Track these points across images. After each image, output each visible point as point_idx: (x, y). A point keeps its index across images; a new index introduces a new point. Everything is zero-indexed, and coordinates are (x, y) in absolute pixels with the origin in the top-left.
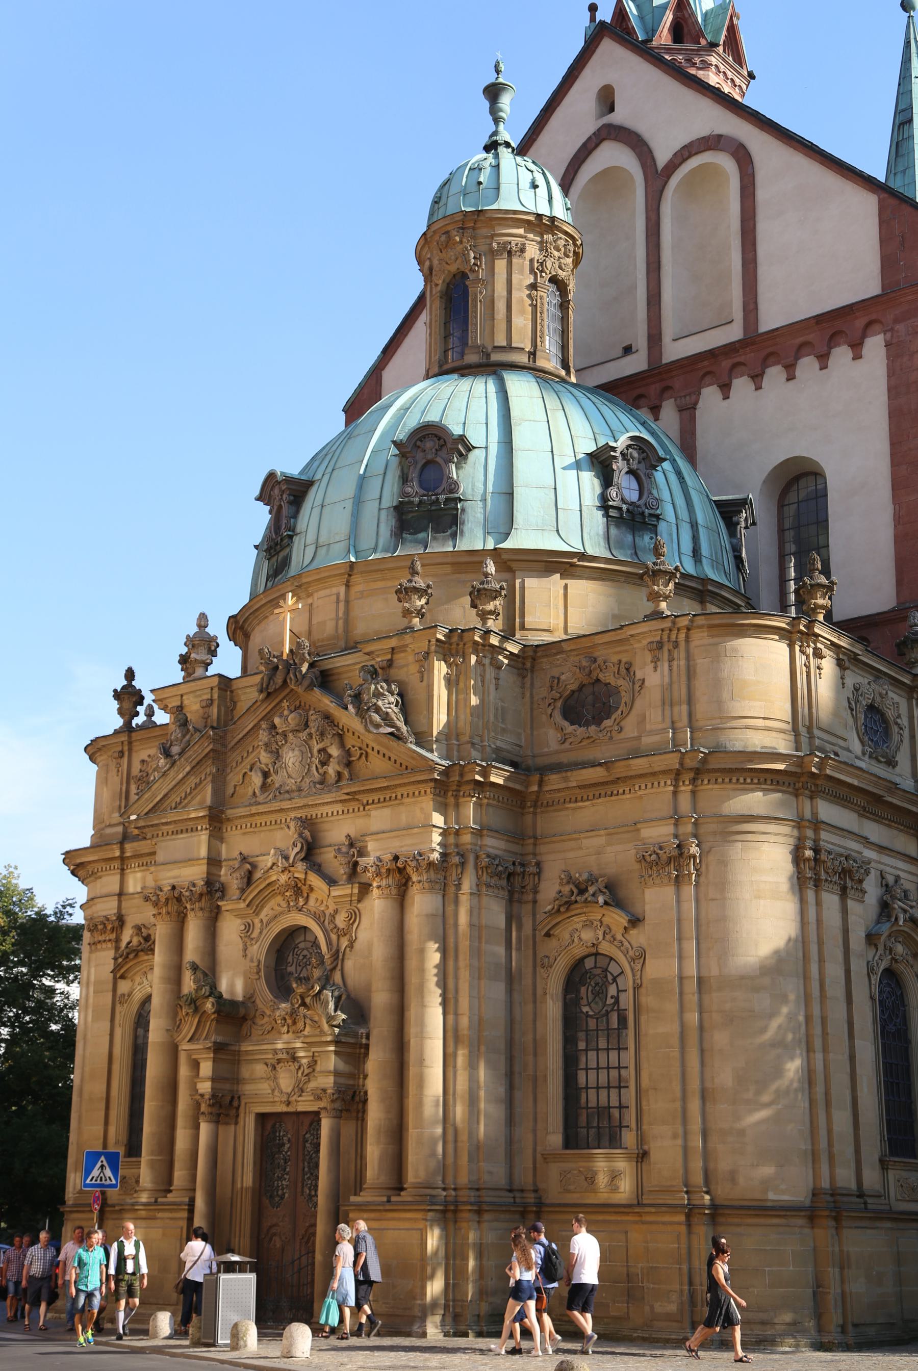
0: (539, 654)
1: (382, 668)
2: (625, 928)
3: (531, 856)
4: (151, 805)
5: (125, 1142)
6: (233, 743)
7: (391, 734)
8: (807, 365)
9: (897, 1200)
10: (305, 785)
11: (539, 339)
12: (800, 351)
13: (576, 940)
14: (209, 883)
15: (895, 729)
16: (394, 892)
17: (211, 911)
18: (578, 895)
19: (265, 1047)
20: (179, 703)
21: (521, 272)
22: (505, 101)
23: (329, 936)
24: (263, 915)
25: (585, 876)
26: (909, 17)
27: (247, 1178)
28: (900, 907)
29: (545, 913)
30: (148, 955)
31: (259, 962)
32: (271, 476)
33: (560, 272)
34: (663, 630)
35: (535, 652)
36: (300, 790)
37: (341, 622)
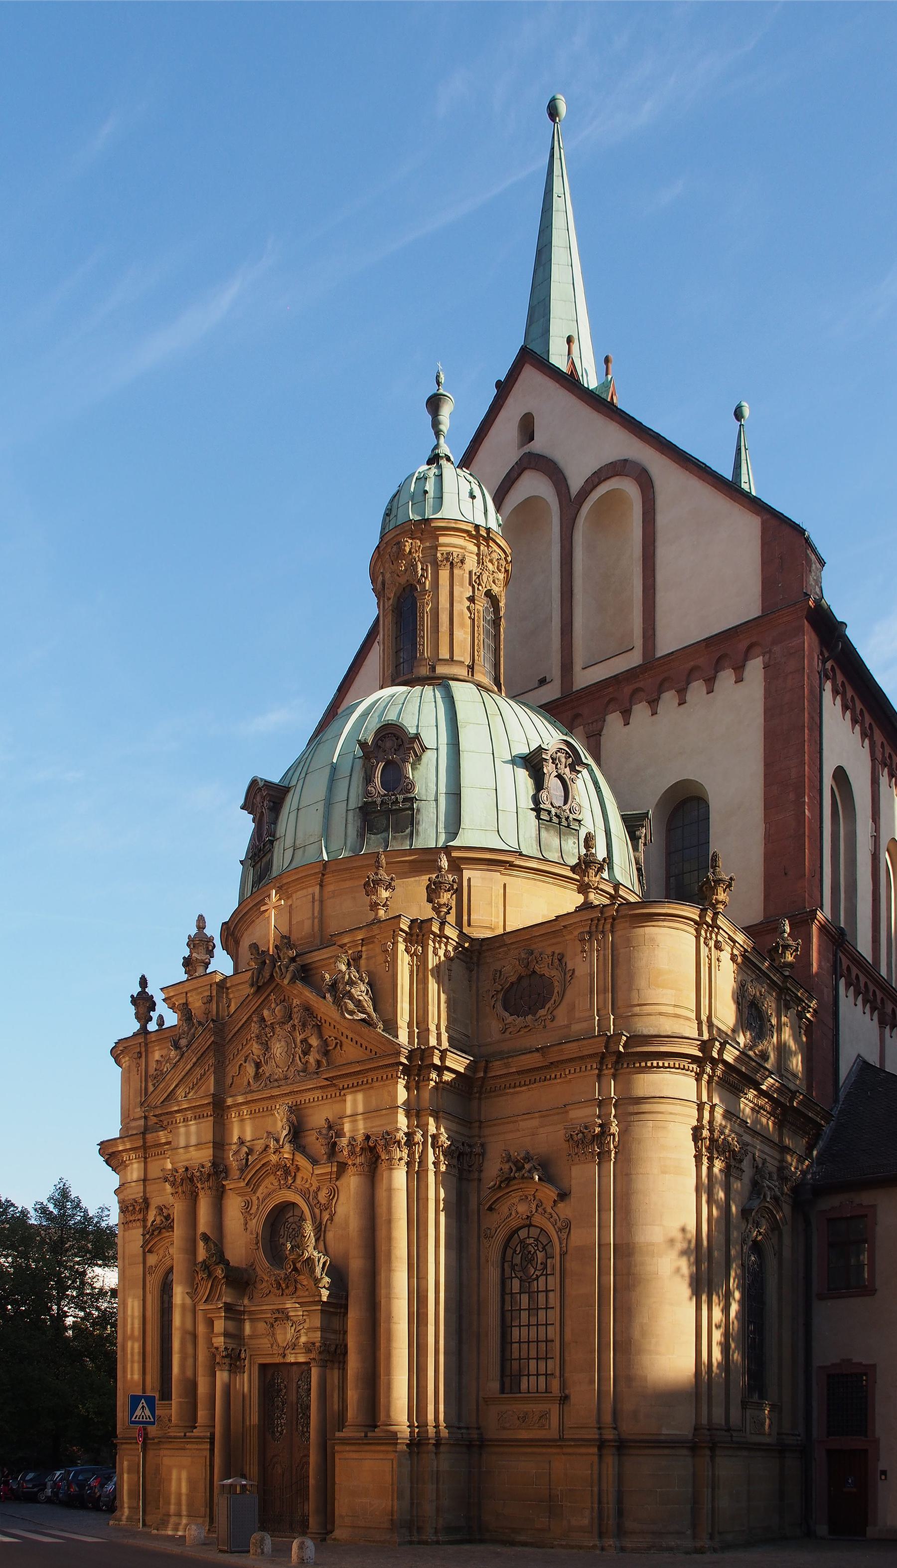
0: (484, 948)
1: (353, 960)
2: (555, 1201)
3: (477, 1138)
4: (166, 1095)
5: (159, 1389)
6: (230, 1036)
7: (363, 1020)
8: (697, 688)
9: (751, 1434)
10: (291, 1074)
11: (476, 653)
13: (513, 1214)
14: (214, 1164)
16: (366, 1169)
17: (217, 1190)
18: (516, 1172)
19: (264, 1308)
21: (462, 585)
22: (446, 412)
23: (313, 1210)
24: (258, 1194)
25: (522, 1155)
26: (740, 425)
27: (254, 1418)
28: (768, 1186)
29: (489, 1188)
30: (169, 1232)
31: (258, 1234)
32: (254, 782)
34: (592, 920)
35: (481, 946)
36: (286, 1078)
37: (316, 920)
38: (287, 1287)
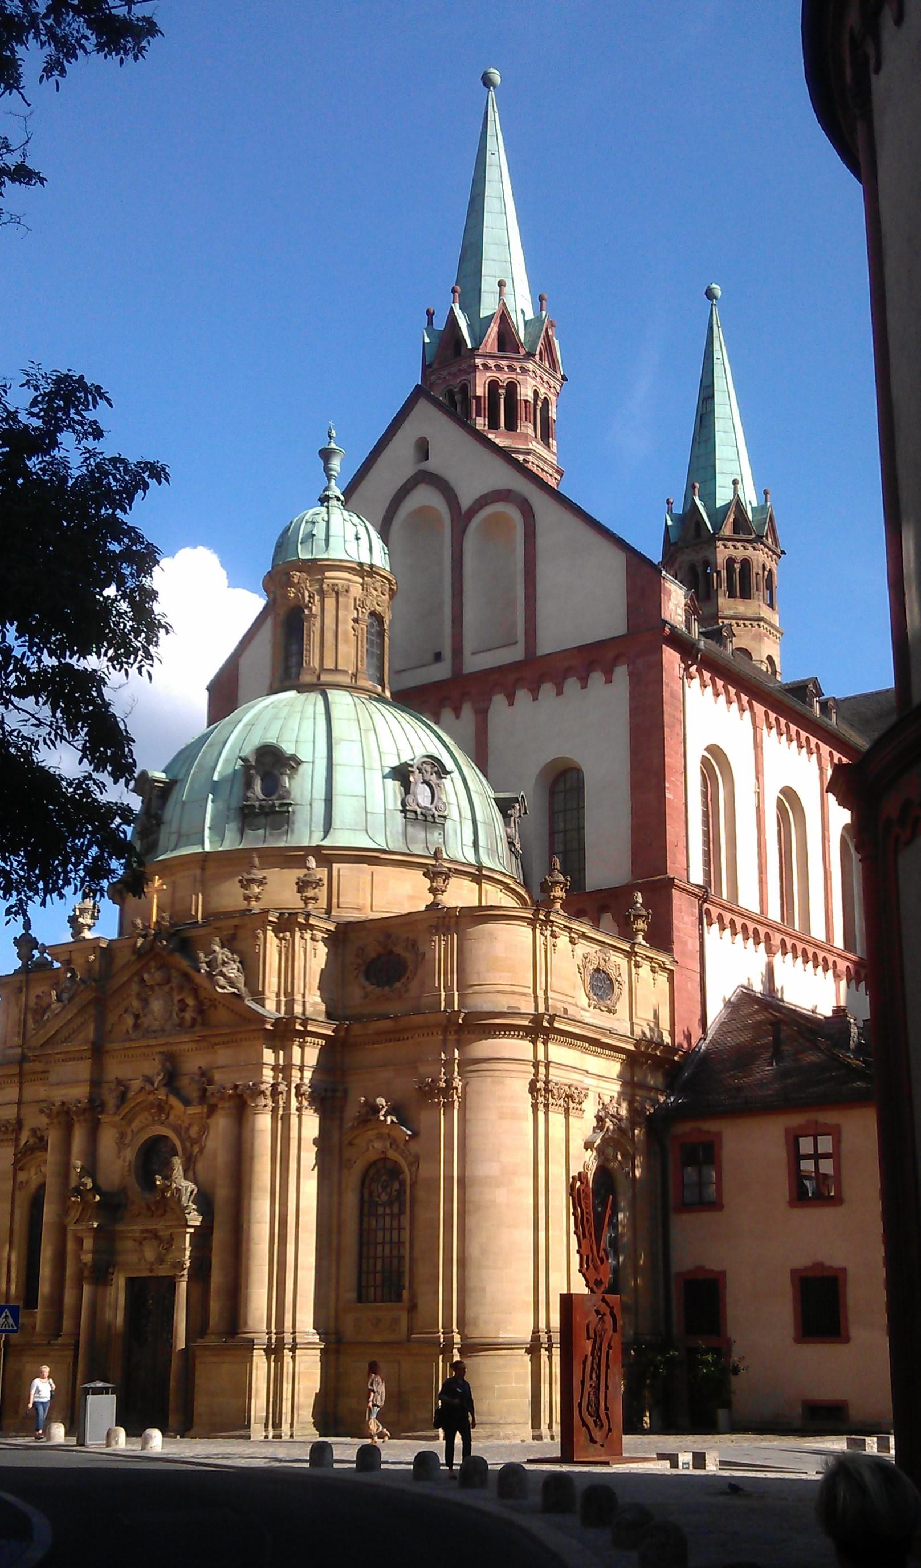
1: (227, 940)
8: (572, 684)
12: (566, 674)
13: (370, 1148)
14: (91, 1100)
15: (616, 985)
20: (67, 958)
22: (336, 464)
33: (377, 607)
36: (163, 1030)
38: (157, 1209)
